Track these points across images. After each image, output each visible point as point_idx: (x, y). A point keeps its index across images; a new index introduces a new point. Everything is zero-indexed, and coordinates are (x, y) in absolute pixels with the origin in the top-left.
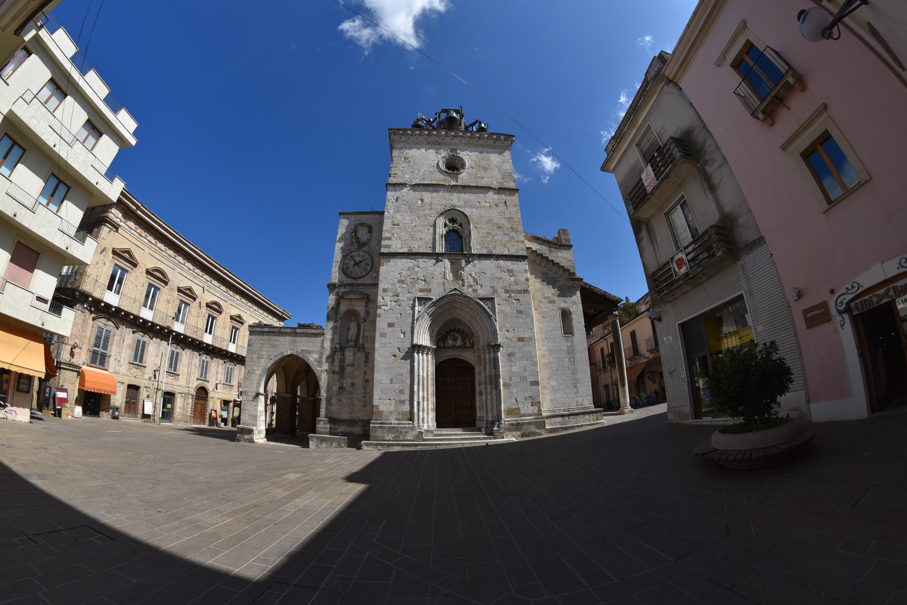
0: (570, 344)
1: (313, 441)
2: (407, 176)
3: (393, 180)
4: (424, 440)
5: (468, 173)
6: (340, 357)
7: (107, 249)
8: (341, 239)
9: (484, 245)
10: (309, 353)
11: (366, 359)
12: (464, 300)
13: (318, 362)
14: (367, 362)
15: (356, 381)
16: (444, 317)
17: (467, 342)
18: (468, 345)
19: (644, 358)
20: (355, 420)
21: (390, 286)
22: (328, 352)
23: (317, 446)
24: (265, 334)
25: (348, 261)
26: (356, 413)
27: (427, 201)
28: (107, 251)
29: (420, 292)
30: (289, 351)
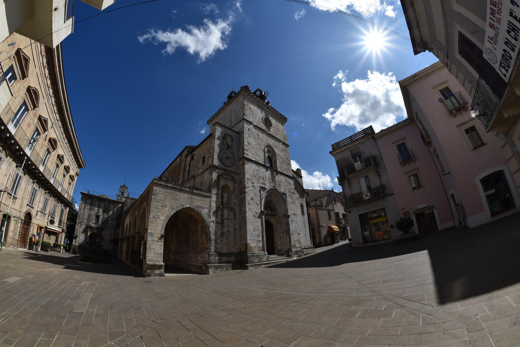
1: (211, 269)
4: (270, 261)
7: (16, 44)
8: (218, 139)
13: (208, 215)
22: (214, 209)
23: (214, 272)
24: (168, 188)
27: (260, 137)
28: (14, 47)
30: (188, 204)
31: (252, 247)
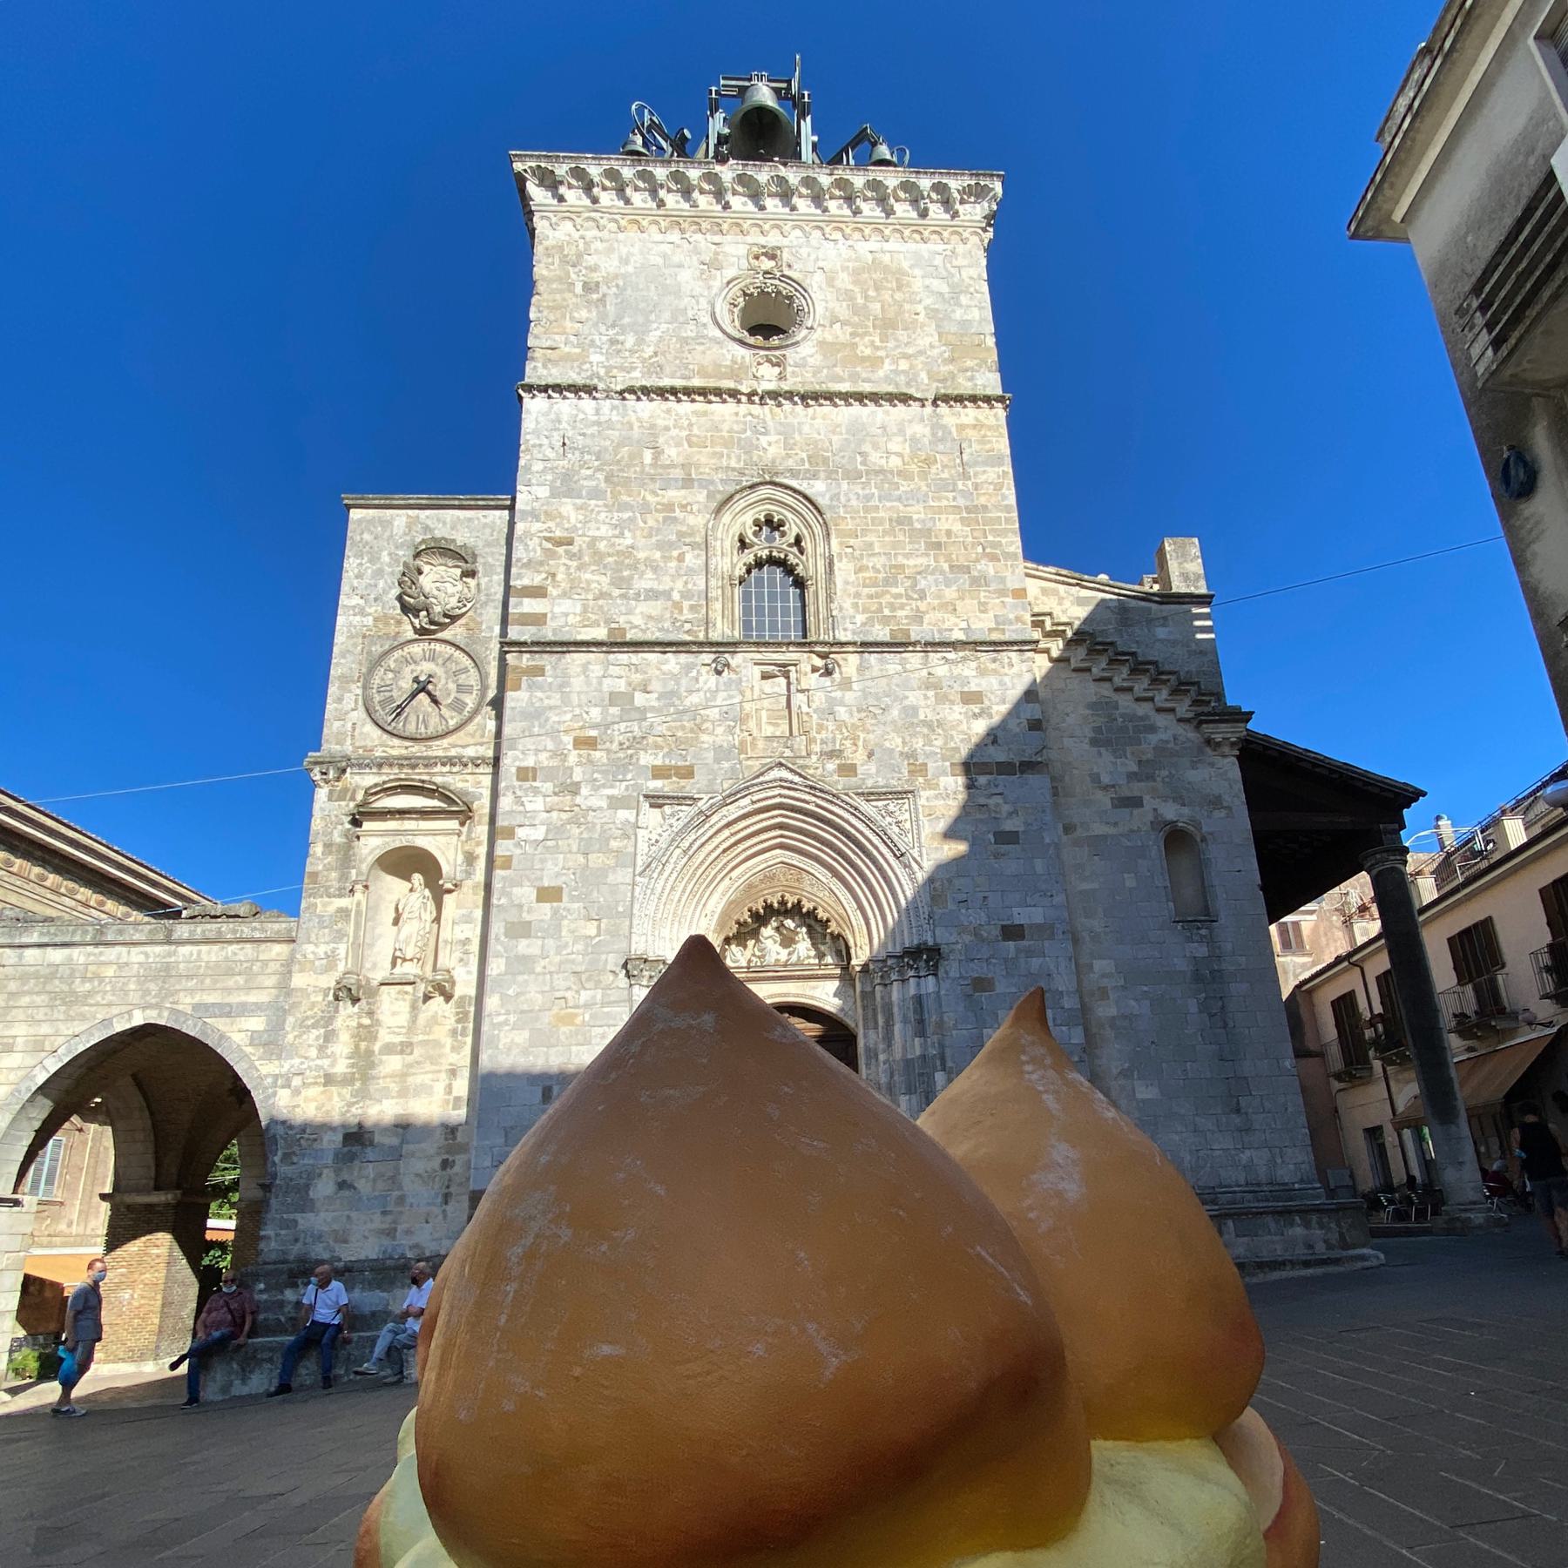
0: (1202, 951)
2: (595, 358)
3: (542, 371)
5: (822, 344)
9: (880, 610)
10: (228, 1015)
11: (458, 1021)
19: (1530, 1024)
25: (390, 675)
26: (408, 1232)
29: (655, 777)
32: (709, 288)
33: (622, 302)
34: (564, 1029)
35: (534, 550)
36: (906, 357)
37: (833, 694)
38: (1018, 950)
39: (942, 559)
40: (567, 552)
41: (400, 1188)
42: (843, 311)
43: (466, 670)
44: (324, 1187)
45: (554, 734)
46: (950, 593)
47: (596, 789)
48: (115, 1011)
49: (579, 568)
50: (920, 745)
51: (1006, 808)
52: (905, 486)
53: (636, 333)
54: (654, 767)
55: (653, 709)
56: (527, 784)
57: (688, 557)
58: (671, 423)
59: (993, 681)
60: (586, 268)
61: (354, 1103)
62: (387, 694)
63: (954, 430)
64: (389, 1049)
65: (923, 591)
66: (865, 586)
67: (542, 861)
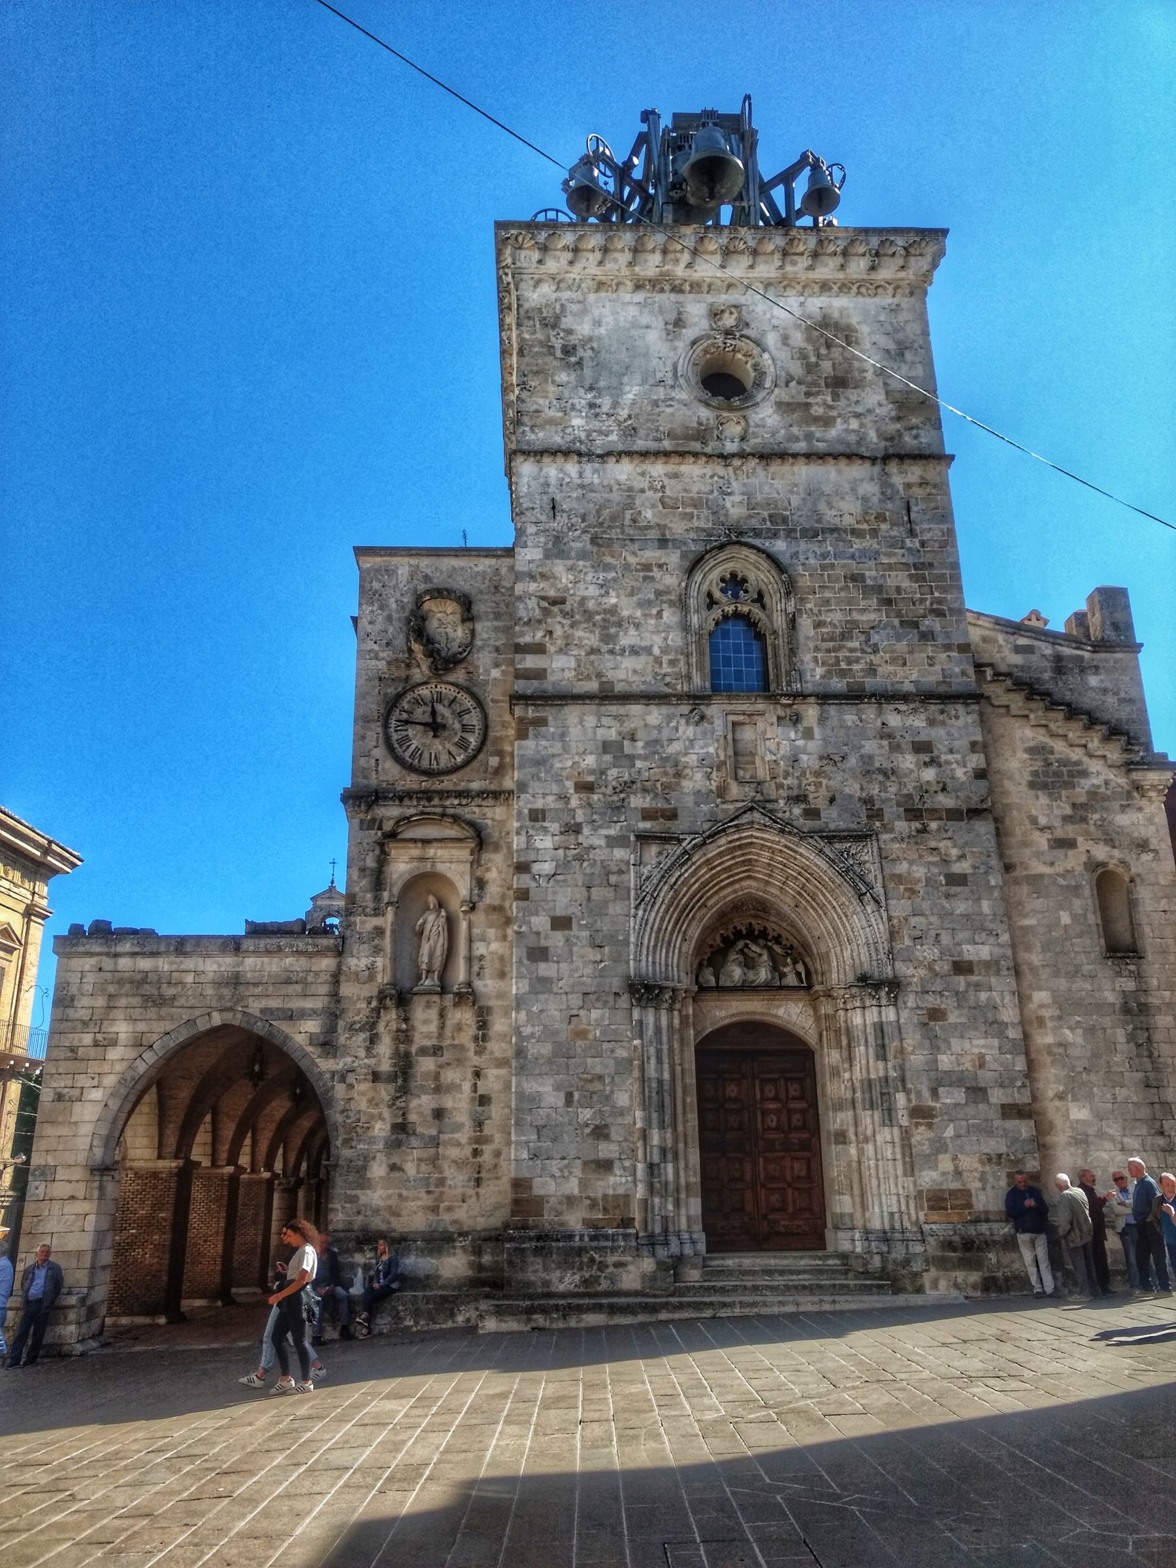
0: (1130, 985)
3: (531, 436)
6: (394, 1026)
10: (291, 1018)
11: (479, 1028)
12: (778, 843)
14: (485, 1038)
15: (448, 1102)
16: (716, 892)
17: (786, 970)
18: (791, 980)
20: (446, 1231)
21: (550, 802)
31: (542, 1197)
32: (675, 349)
33: (597, 365)
34: (579, 1043)
35: (533, 609)
36: (858, 416)
37: (797, 743)
38: (968, 985)
39: (893, 614)
40: (561, 611)
41: (441, 1172)
42: (796, 369)
43: (468, 711)
44: (378, 1170)
45: (558, 780)
46: (902, 646)
47: (595, 829)
48: (197, 1013)
49: (572, 626)
50: (876, 791)
51: (954, 852)
52: (858, 544)
53: (611, 395)
54: (643, 810)
55: (640, 757)
56: (538, 825)
57: (666, 614)
58: (646, 485)
59: (941, 732)
60: (564, 330)
61: (397, 1098)
62: (404, 733)
63: (901, 488)
64: (423, 1051)
65: (876, 645)
66: (823, 640)
67: (555, 893)
